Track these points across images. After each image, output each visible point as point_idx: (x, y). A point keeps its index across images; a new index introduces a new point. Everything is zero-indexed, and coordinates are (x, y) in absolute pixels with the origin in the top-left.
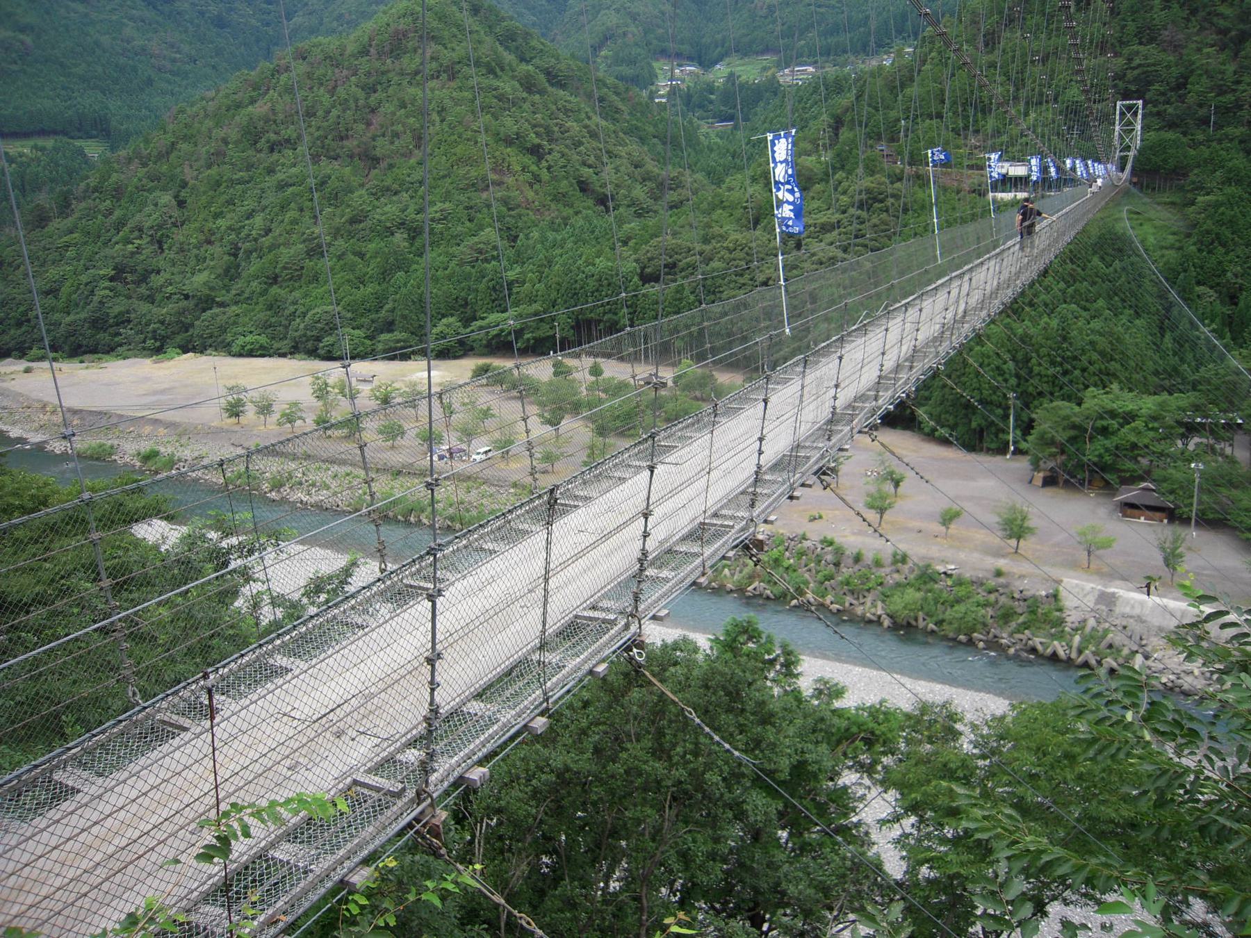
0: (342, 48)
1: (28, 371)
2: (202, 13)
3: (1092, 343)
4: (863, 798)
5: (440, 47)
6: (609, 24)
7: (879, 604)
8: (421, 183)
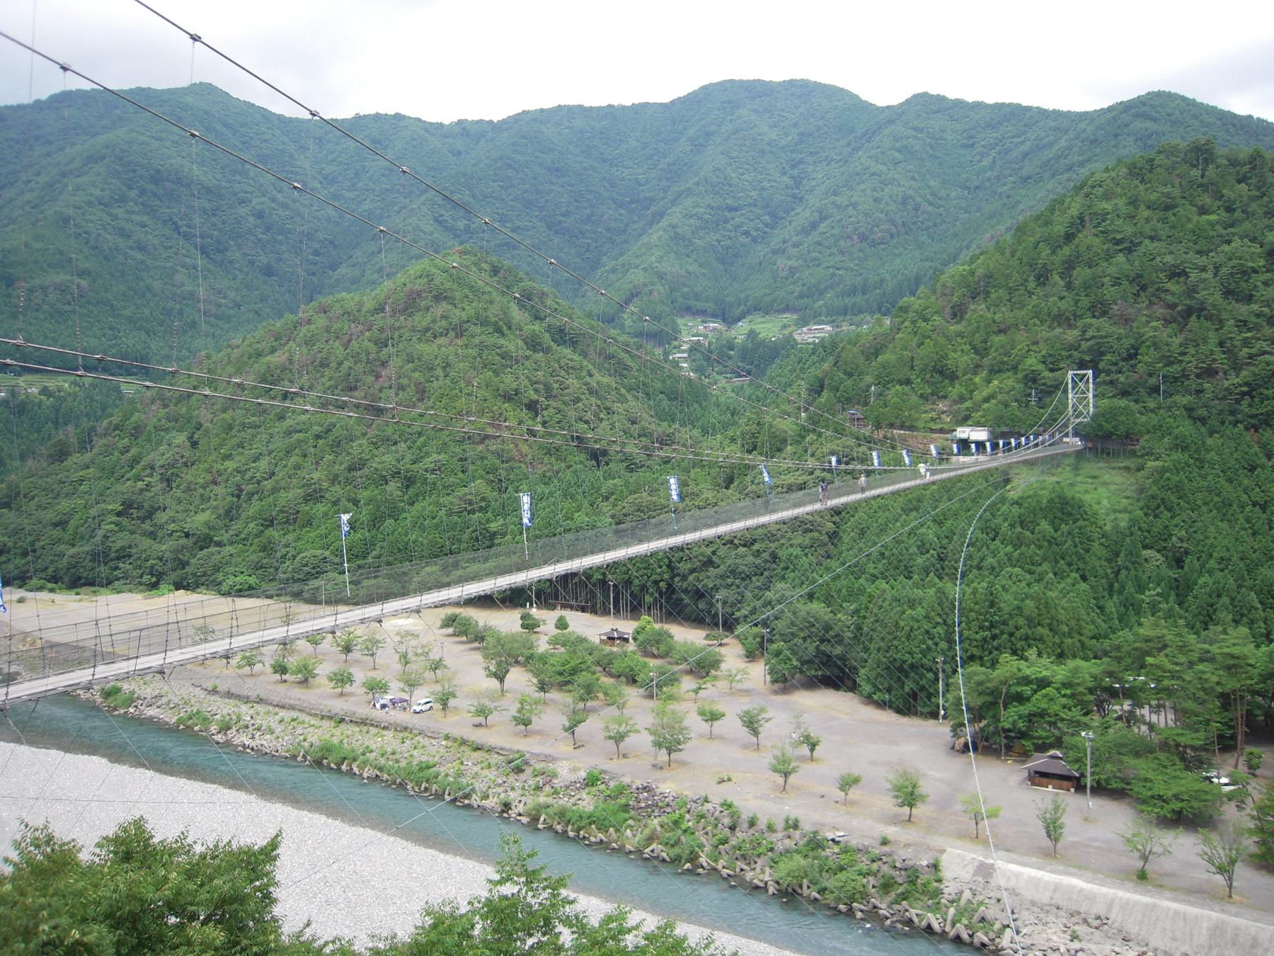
0: (360, 305)
1: (21, 601)
5: (451, 307)
7: (767, 870)
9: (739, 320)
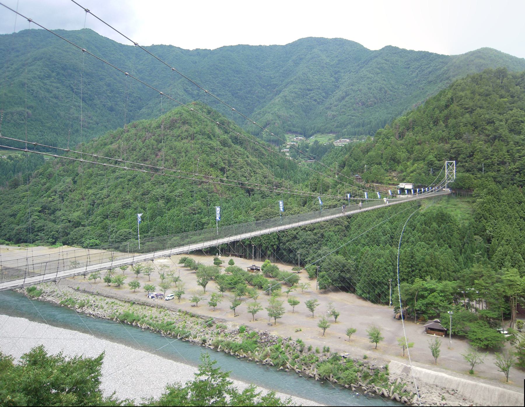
0: (151, 124)
2: (104, 105)
5: (189, 127)
6: (269, 119)
7: (315, 369)
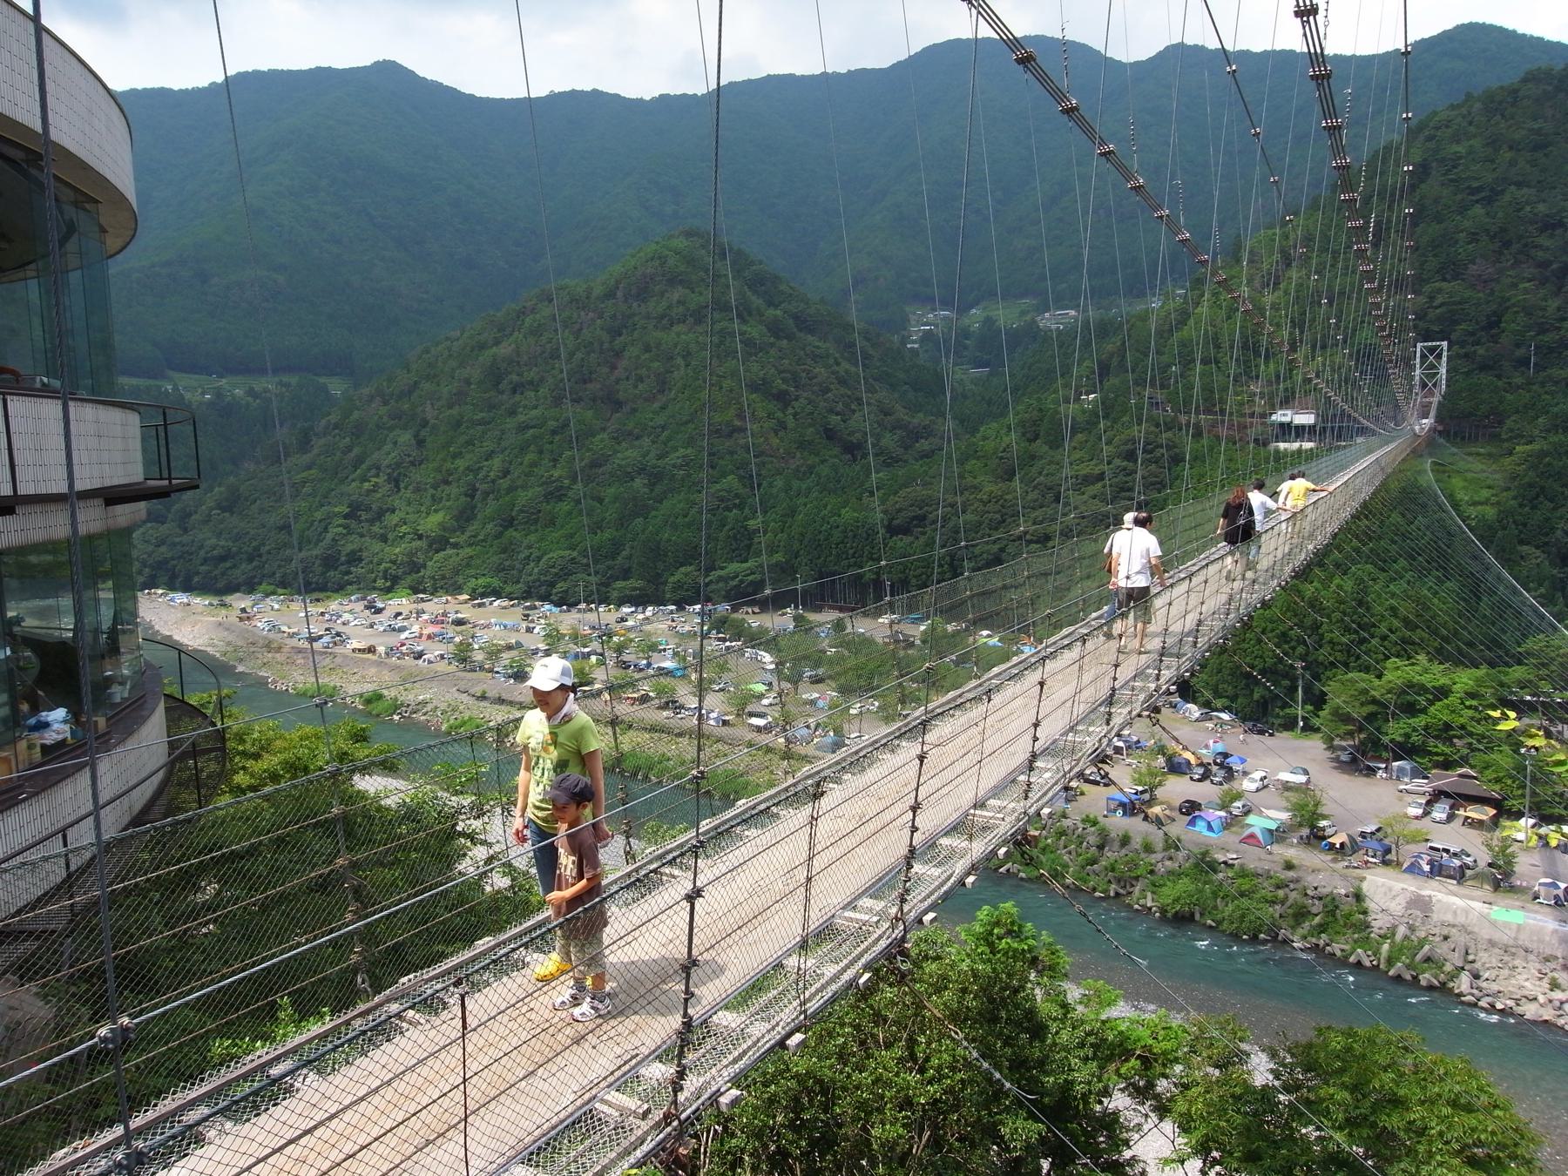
0: (589, 291)
3: (1393, 609)
4: (1139, 1127)
7: (1149, 895)
8: (663, 428)
9: (972, 307)
